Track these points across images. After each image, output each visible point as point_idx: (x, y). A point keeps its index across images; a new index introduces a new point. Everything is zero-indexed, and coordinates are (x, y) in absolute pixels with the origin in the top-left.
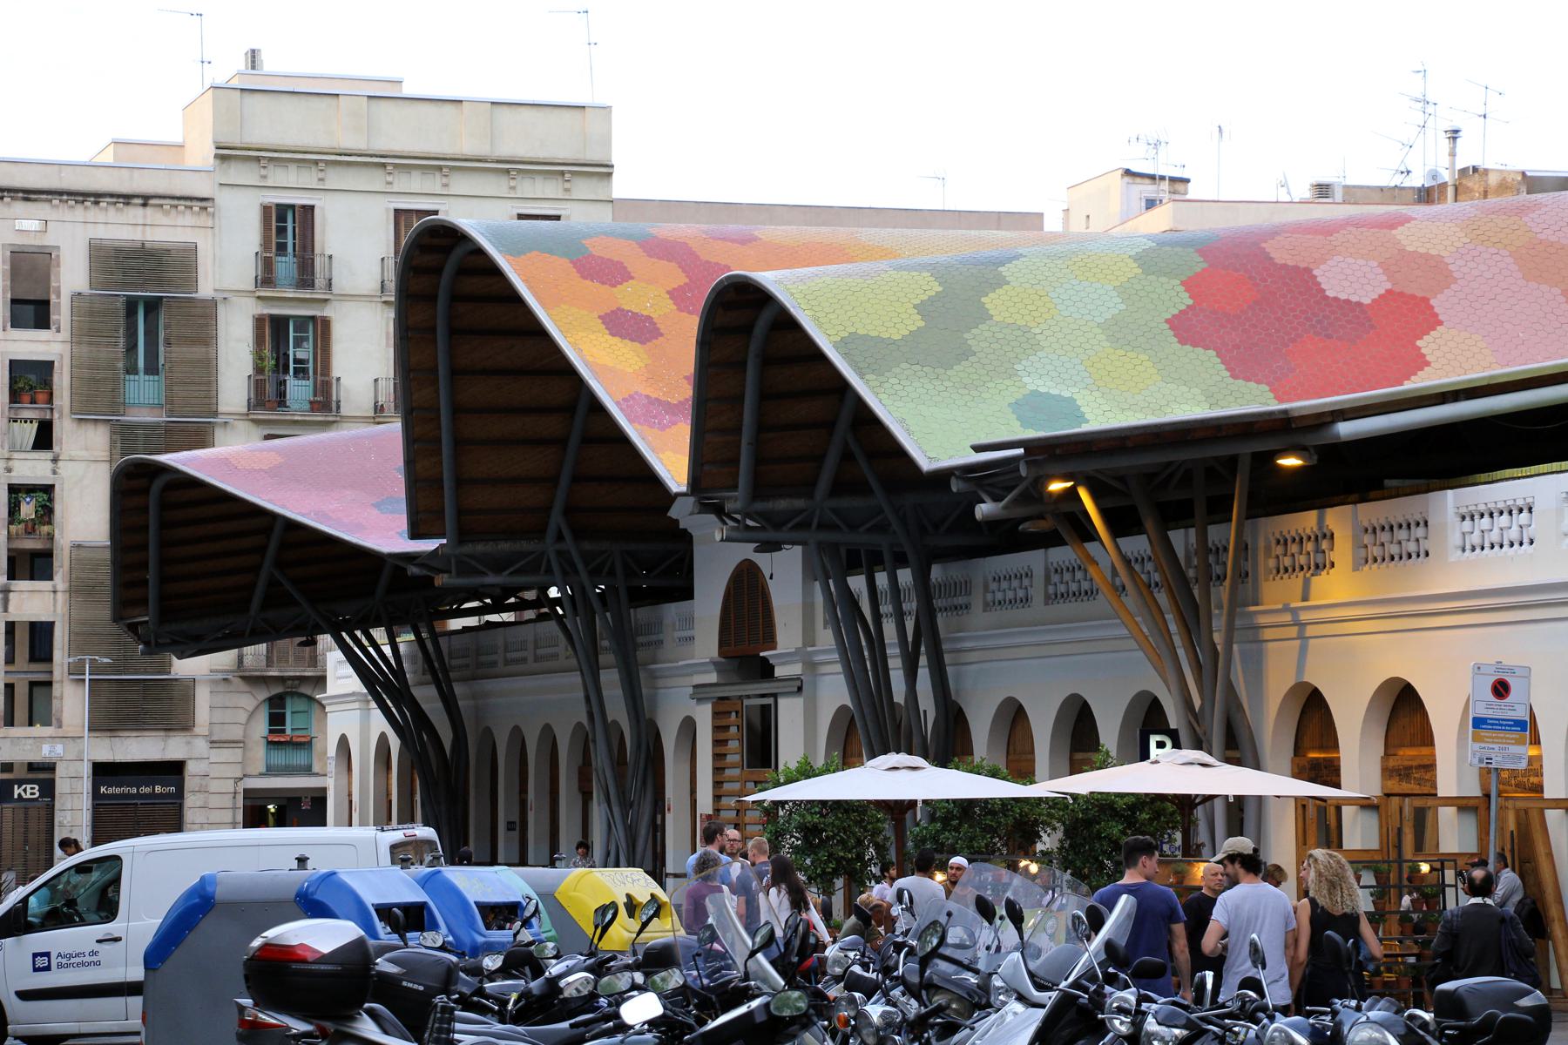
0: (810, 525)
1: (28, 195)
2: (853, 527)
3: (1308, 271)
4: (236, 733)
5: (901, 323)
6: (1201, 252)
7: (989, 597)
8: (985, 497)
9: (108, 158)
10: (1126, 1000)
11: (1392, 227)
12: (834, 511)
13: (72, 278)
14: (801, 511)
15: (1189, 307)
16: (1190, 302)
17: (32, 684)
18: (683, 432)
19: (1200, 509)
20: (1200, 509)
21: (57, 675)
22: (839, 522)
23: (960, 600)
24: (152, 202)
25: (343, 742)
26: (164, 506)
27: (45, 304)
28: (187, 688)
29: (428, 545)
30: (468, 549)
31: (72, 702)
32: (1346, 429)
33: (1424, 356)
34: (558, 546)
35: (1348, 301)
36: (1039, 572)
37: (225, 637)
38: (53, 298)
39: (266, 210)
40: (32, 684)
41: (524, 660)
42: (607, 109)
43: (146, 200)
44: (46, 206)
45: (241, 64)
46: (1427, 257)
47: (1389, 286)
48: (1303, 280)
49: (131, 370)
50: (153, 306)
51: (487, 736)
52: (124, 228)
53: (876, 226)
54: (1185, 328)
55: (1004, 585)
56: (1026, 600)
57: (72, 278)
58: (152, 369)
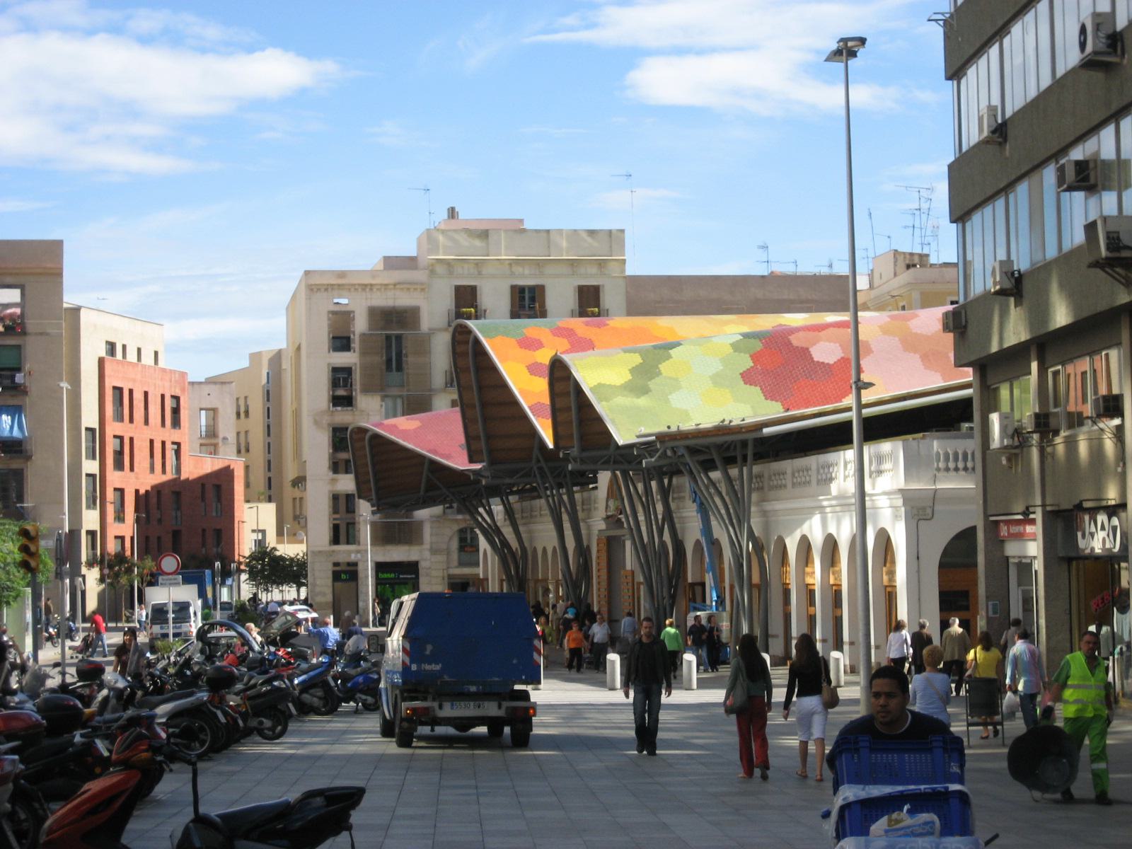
2: (629, 462)
3: (807, 349)
7: (771, 483)
8: (647, 455)
10: (220, 662)
13: (360, 325)
19: (739, 459)
20: (739, 459)
24: (398, 286)
25: (485, 551)
26: (372, 447)
27: (348, 339)
28: (420, 524)
29: (477, 466)
31: (366, 533)
32: (766, 431)
36: (814, 467)
38: (352, 336)
39: (513, 288)
45: (445, 216)
47: (843, 355)
48: (804, 353)
50: (399, 338)
51: (535, 550)
54: (748, 377)
55: (777, 477)
56: (809, 482)
57: (360, 325)
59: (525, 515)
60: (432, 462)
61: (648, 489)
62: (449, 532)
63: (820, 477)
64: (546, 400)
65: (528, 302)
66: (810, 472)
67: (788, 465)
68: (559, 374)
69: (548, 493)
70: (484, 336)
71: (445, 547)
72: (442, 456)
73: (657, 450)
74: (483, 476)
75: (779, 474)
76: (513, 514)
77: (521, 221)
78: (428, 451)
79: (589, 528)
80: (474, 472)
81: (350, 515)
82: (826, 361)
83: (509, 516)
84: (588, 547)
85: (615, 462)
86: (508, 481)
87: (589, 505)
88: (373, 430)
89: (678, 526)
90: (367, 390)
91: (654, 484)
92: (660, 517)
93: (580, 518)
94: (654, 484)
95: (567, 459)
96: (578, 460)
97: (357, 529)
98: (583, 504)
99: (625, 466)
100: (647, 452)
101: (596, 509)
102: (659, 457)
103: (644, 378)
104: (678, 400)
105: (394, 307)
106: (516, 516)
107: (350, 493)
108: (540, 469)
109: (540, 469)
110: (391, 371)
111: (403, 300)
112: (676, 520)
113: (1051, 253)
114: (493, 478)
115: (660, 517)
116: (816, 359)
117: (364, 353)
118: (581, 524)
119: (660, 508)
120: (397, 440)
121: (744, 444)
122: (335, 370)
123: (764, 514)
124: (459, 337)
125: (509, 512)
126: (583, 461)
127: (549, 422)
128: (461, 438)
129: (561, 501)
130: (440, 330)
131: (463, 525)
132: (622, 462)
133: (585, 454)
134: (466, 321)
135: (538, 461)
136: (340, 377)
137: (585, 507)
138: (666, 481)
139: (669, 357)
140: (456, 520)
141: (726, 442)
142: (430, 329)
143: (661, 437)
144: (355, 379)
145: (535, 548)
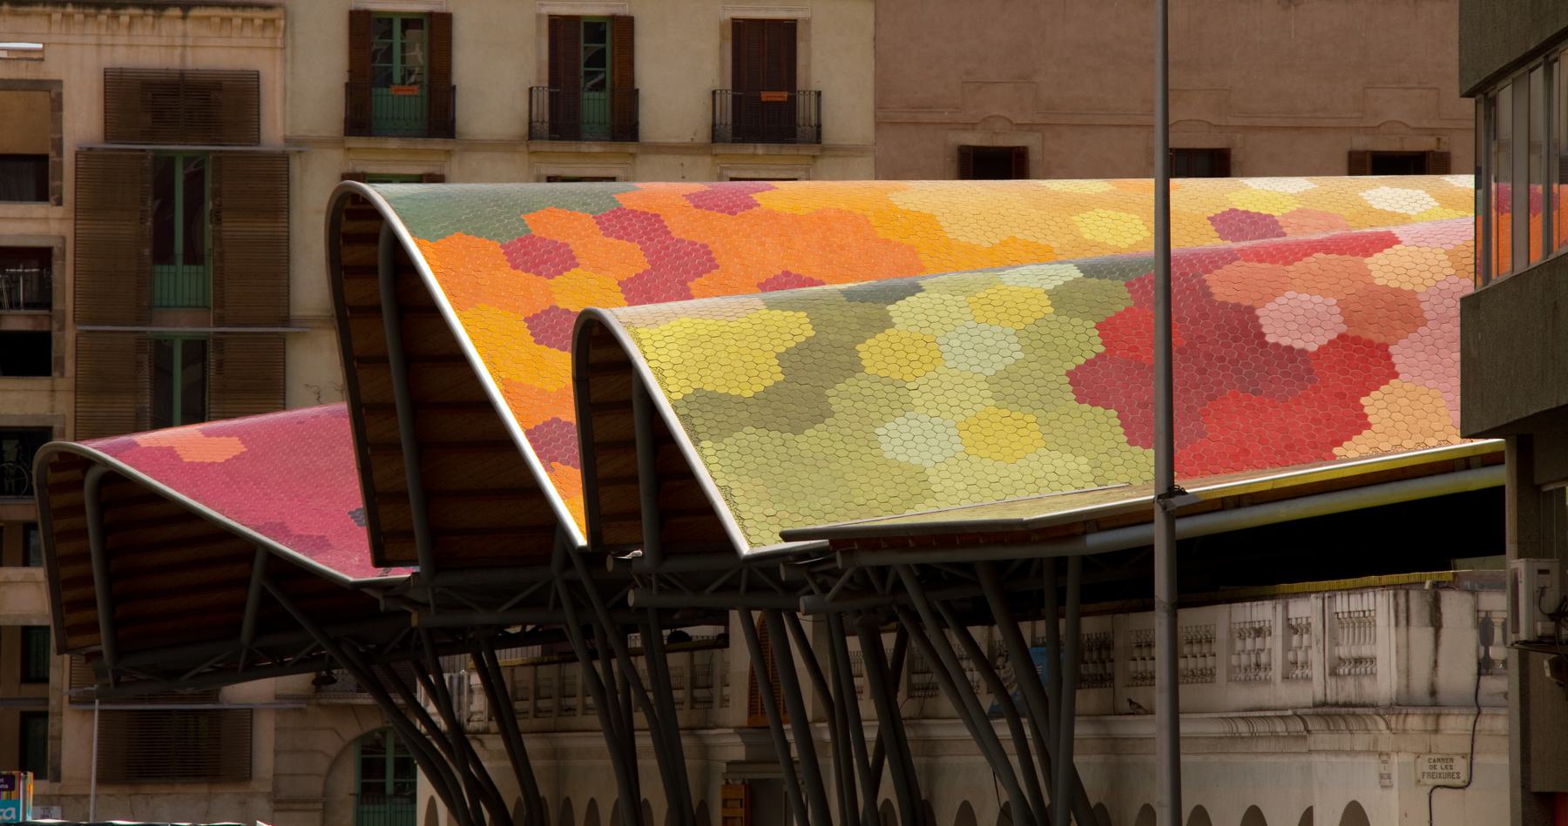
0: (737, 588)
3: (1251, 310)
4: (316, 787)
5: (756, 374)
11: (1367, 253)
15: (1098, 356)
16: (1101, 349)
21: (53, 702)
24: (195, 12)
26: (102, 506)
28: (245, 717)
32: (1096, 541)
33: (1366, 416)
35: (1290, 349)
44: (43, 22)
46: (1397, 292)
47: (1344, 329)
48: (1242, 325)
49: (163, 254)
51: (568, 804)
54: (1088, 384)
57: (83, 122)
58: (193, 256)
59: (542, 704)
60: (273, 556)
62: (333, 740)
64: (569, 415)
68: (599, 356)
70: (413, 234)
71: (316, 787)
72: (299, 542)
73: (837, 574)
78: (256, 529)
79: (705, 751)
81: (32, 690)
82: (1298, 345)
83: (501, 721)
84: (704, 806)
85: (752, 588)
88: (106, 463)
91: (854, 644)
94: (854, 644)
97: (51, 731)
100: (813, 575)
101: (725, 701)
102: (844, 589)
103: (805, 390)
104: (900, 440)
105: (182, 73)
107: (35, 622)
108: (573, 586)
113: (1537, 258)
116: (1270, 339)
118: (686, 741)
124: (349, 226)
127: (575, 475)
128: (357, 501)
130: (321, 142)
139: (886, 323)
141: (1011, 561)
142: (286, 140)
145: (568, 802)
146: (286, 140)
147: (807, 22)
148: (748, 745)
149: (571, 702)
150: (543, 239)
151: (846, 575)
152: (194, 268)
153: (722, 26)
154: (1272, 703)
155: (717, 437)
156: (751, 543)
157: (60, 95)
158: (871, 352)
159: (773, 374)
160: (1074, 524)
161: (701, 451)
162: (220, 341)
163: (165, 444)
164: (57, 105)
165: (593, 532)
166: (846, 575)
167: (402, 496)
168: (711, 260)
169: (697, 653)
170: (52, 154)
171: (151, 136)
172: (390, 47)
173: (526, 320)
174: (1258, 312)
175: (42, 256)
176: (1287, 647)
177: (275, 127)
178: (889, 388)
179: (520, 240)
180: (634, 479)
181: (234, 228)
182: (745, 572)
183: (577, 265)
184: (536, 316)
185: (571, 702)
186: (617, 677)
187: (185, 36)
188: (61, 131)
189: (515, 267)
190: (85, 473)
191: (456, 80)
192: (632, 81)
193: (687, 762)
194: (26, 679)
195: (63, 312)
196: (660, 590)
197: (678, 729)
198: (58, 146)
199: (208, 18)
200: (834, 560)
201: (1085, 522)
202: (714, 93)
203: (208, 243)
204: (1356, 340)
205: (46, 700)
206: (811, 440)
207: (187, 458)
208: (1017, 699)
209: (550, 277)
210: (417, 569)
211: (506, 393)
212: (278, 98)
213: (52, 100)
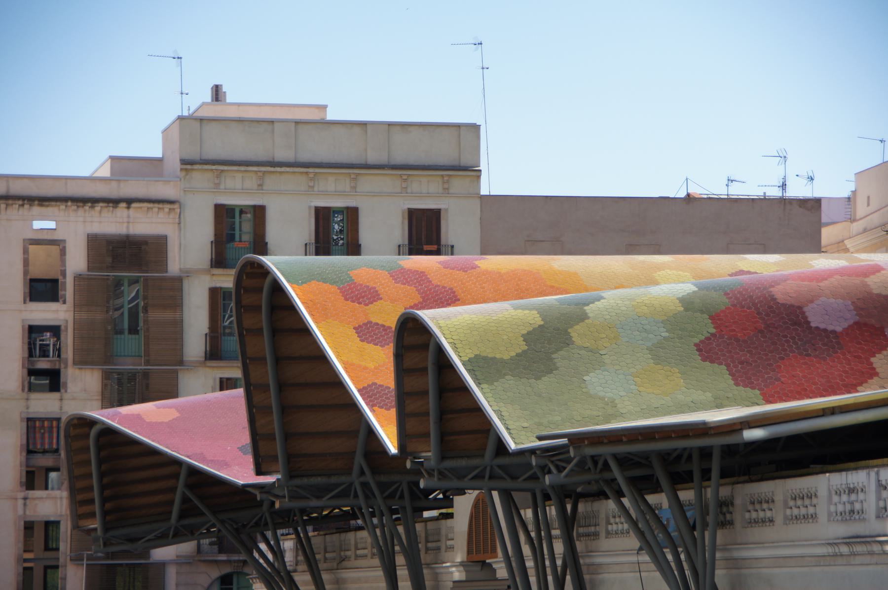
0: (484, 477)
1: (43, 201)
2: (514, 478)
6: (726, 294)
7: (610, 527)
9: (105, 172)
12: (499, 466)
14: (476, 468)
16: (713, 331)
17: (46, 568)
18: (393, 412)
19: (697, 475)
20: (697, 475)
21: (61, 560)
22: (504, 476)
23: (592, 529)
24: (134, 205)
26: (99, 448)
30: (298, 481)
34: (362, 479)
35: (825, 330)
37: (158, 538)
40: (46, 568)
41: (365, 556)
42: (475, 128)
43: (130, 202)
45: (208, 97)
52: (112, 223)
53: (431, 308)
54: (707, 351)
57: (77, 261)
61: (542, 523)
63: (832, 508)
64: (388, 380)
65: (335, 233)
66: (731, 509)
67: (781, 489)
69: (375, 521)
73: (569, 461)
74: (277, 496)
75: (760, 503)
76: (314, 554)
77: (324, 108)
78: (188, 457)
79: (436, 577)
80: (260, 487)
82: (830, 328)
86: (314, 503)
87: (437, 545)
88: (103, 423)
89: (586, 577)
90: (82, 361)
92: (559, 562)
93: (423, 561)
95: (417, 472)
96: (436, 474)
98: (427, 541)
99: (508, 484)
100: (552, 462)
102: (572, 470)
106: (318, 557)
107: (52, 519)
108: (365, 485)
109: (365, 485)
110: (121, 332)
111: (142, 224)
112: (584, 569)
114: (292, 498)
115: (559, 562)
116: (813, 325)
117: (76, 306)
118: (425, 571)
119: (559, 547)
120: (144, 439)
121: (705, 453)
122: (33, 330)
123: (735, 564)
125: (304, 548)
126: (442, 475)
128: (245, 438)
129: (394, 534)
130: (198, 272)
131: (227, 570)
132: (502, 478)
133: (449, 464)
134: (260, 257)
135: (362, 473)
136: (37, 337)
137: (430, 545)
138: (569, 507)
140: (216, 562)
141: (676, 450)
143: (576, 439)
144: (66, 344)
146: (181, 270)
147: (446, 210)
148: (467, 571)
149: (348, 553)
150: (361, 285)
151: (575, 461)
152: (133, 336)
153: (403, 213)
154: (867, 533)
155: (490, 382)
156: (515, 443)
157: (64, 248)
158: (575, 332)
159: (521, 346)
160: (734, 424)
161: (482, 390)
162: (146, 374)
163: (136, 413)
164: (63, 252)
165: (402, 446)
166: (575, 461)
167: (272, 437)
168: (456, 296)
169: (429, 523)
170: (60, 278)
171: (113, 268)
172: (234, 223)
173: (355, 328)
174: (805, 309)
175: (55, 330)
176: (879, 498)
177: (174, 266)
178: (590, 353)
179: (349, 285)
180: (427, 414)
181: (155, 315)
182: (488, 469)
183: (381, 299)
184: (360, 326)
185: (348, 553)
186: (380, 538)
187: (129, 217)
188: (65, 266)
189: (346, 299)
190: (91, 428)
191: (267, 240)
192: (357, 240)
193: (427, 583)
194: (47, 548)
195: (67, 359)
196: (439, 479)
197: (421, 565)
198: (64, 273)
199: (141, 208)
200: (568, 452)
201: (741, 423)
202: (399, 246)
203: (141, 324)
204: (865, 324)
205: (58, 559)
206: (546, 383)
207: (144, 421)
208: (674, 534)
209: (366, 305)
210: (279, 476)
211: (345, 369)
212: (176, 249)
213: (61, 250)
